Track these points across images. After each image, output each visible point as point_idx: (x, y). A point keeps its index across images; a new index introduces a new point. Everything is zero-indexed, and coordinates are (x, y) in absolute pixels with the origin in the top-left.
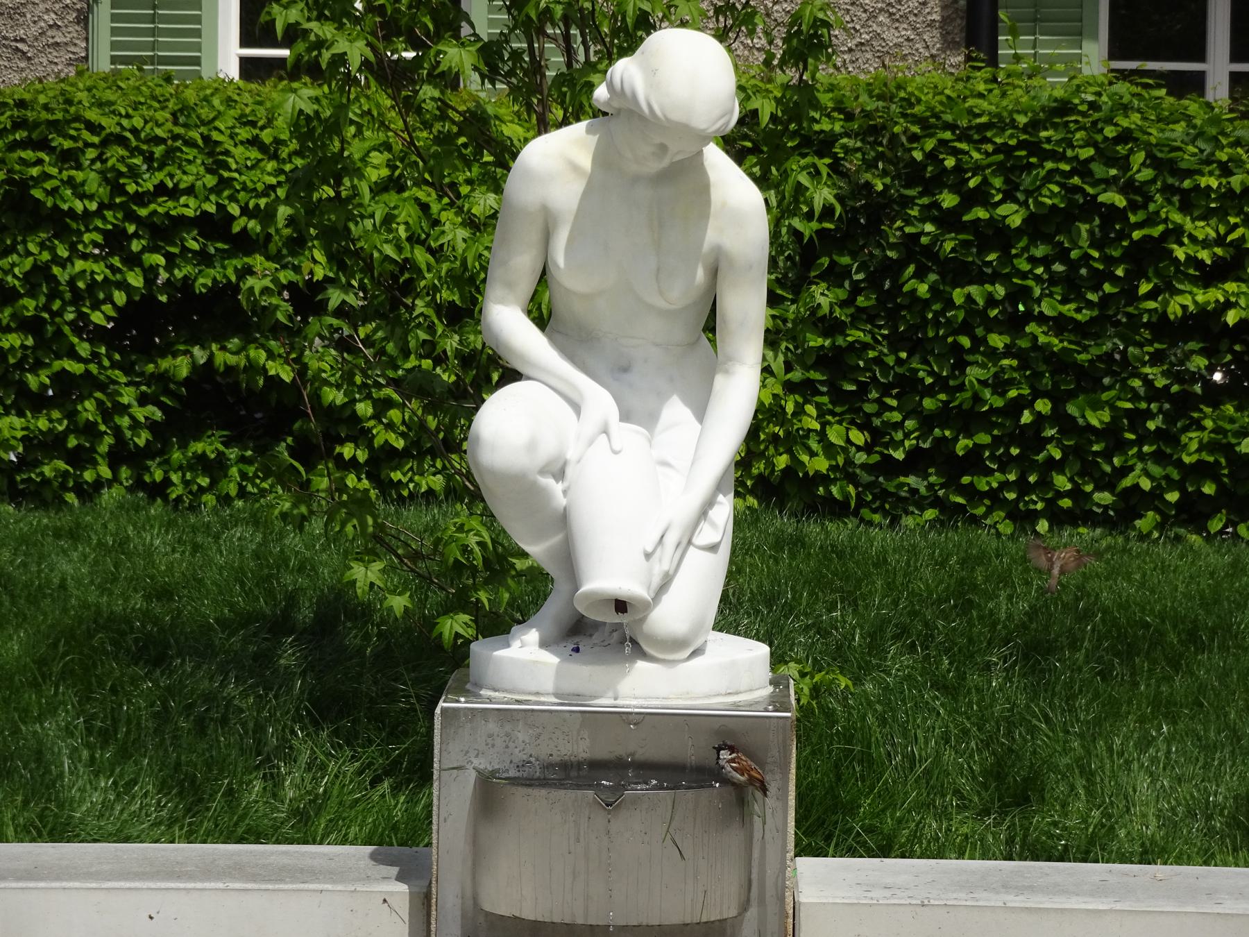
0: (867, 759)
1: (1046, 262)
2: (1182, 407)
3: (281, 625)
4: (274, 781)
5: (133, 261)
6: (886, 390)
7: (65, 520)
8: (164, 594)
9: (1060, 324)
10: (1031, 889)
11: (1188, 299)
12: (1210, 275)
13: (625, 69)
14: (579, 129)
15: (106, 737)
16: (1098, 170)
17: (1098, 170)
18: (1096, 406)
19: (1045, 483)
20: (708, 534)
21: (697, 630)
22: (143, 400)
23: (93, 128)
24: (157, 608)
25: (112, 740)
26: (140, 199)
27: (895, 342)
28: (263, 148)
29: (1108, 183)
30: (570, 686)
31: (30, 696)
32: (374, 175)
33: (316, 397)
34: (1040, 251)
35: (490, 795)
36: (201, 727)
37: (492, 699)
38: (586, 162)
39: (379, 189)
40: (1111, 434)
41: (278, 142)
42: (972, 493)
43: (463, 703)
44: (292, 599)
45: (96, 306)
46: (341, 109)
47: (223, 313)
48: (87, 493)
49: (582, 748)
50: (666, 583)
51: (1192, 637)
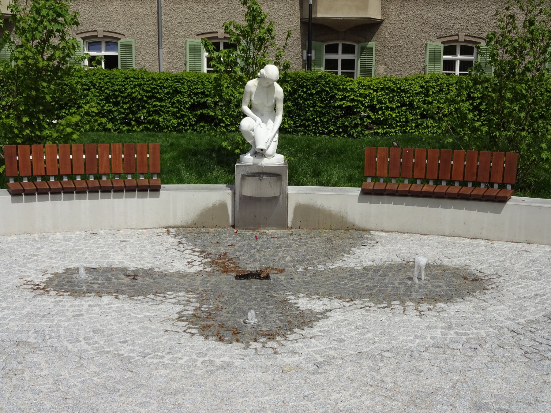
0: (296, 170)
1: (318, 98)
2: (337, 118)
3: (213, 150)
4: (212, 173)
5: (192, 98)
6: (296, 116)
7: (183, 135)
8: (196, 146)
9: (320, 107)
10: (322, 191)
11: (338, 103)
12: (341, 100)
13: (262, 71)
14: (256, 79)
15: (188, 167)
16: (326, 85)
17: (326, 85)
18: (325, 118)
19: (318, 129)
20: (275, 139)
21: (273, 153)
22: (193, 118)
23: (186, 80)
24: (195, 148)
25: (189, 167)
26: (193, 89)
27: (297, 109)
29: (327, 87)
31: (177, 161)
32: (225, 86)
33: (217, 117)
34: (317, 97)
35: (243, 177)
36: (202, 166)
37: (244, 164)
38: (257, 85)
39: (226, 88)
40: (327, 122)
42: (308, 130)
43: (239, 164)
44: (214, 146)
46: (221, 77)
47: (204, 105)
48: (186, 131)
49: (257, 171)
50: (268, 147)
51: (341, 152)
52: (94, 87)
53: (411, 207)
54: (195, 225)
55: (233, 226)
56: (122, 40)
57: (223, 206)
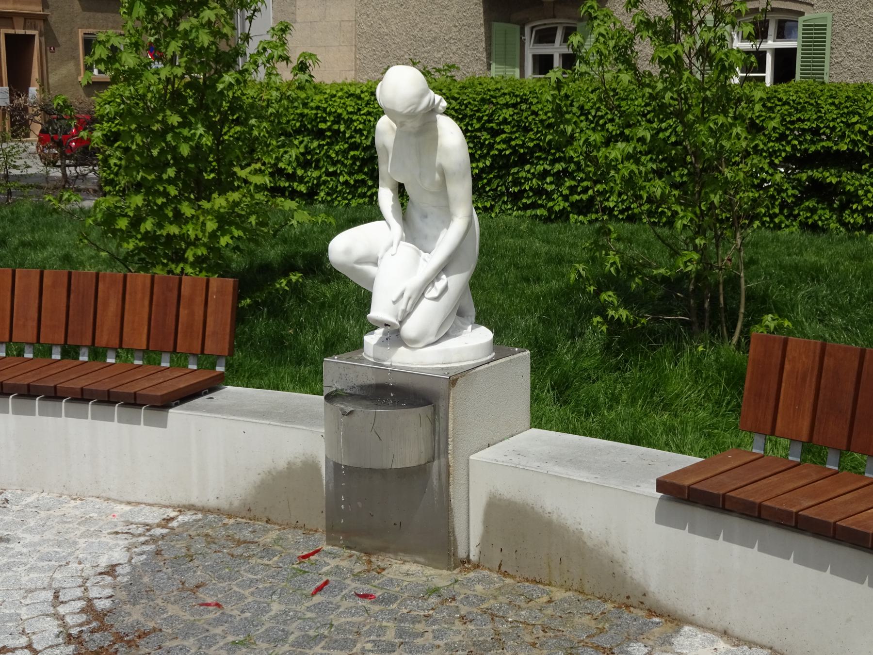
5: (789, 143)
26: (792, 123)
28: (836, 106)
30: (379, 356)
41: (840, 103)
45: (776, 158)
52: (587, 119)
53: (811, 573)
56: (807, 16)
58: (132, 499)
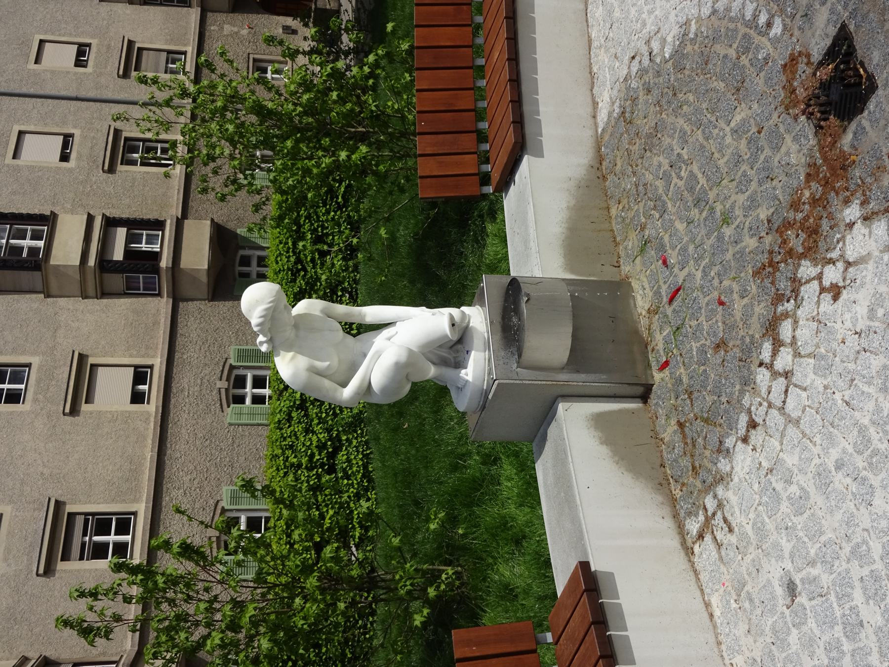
53: (540, 66)
54: (662, 485)
55: (644, 397)
57: (599, 421)
58: (706, 615)
